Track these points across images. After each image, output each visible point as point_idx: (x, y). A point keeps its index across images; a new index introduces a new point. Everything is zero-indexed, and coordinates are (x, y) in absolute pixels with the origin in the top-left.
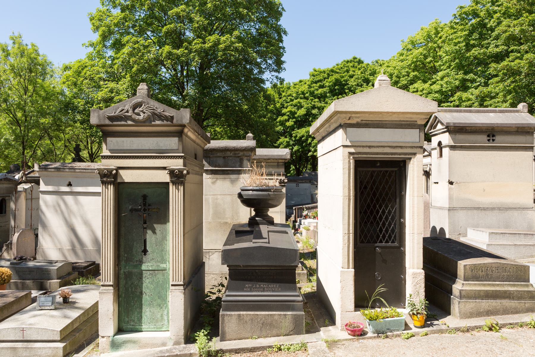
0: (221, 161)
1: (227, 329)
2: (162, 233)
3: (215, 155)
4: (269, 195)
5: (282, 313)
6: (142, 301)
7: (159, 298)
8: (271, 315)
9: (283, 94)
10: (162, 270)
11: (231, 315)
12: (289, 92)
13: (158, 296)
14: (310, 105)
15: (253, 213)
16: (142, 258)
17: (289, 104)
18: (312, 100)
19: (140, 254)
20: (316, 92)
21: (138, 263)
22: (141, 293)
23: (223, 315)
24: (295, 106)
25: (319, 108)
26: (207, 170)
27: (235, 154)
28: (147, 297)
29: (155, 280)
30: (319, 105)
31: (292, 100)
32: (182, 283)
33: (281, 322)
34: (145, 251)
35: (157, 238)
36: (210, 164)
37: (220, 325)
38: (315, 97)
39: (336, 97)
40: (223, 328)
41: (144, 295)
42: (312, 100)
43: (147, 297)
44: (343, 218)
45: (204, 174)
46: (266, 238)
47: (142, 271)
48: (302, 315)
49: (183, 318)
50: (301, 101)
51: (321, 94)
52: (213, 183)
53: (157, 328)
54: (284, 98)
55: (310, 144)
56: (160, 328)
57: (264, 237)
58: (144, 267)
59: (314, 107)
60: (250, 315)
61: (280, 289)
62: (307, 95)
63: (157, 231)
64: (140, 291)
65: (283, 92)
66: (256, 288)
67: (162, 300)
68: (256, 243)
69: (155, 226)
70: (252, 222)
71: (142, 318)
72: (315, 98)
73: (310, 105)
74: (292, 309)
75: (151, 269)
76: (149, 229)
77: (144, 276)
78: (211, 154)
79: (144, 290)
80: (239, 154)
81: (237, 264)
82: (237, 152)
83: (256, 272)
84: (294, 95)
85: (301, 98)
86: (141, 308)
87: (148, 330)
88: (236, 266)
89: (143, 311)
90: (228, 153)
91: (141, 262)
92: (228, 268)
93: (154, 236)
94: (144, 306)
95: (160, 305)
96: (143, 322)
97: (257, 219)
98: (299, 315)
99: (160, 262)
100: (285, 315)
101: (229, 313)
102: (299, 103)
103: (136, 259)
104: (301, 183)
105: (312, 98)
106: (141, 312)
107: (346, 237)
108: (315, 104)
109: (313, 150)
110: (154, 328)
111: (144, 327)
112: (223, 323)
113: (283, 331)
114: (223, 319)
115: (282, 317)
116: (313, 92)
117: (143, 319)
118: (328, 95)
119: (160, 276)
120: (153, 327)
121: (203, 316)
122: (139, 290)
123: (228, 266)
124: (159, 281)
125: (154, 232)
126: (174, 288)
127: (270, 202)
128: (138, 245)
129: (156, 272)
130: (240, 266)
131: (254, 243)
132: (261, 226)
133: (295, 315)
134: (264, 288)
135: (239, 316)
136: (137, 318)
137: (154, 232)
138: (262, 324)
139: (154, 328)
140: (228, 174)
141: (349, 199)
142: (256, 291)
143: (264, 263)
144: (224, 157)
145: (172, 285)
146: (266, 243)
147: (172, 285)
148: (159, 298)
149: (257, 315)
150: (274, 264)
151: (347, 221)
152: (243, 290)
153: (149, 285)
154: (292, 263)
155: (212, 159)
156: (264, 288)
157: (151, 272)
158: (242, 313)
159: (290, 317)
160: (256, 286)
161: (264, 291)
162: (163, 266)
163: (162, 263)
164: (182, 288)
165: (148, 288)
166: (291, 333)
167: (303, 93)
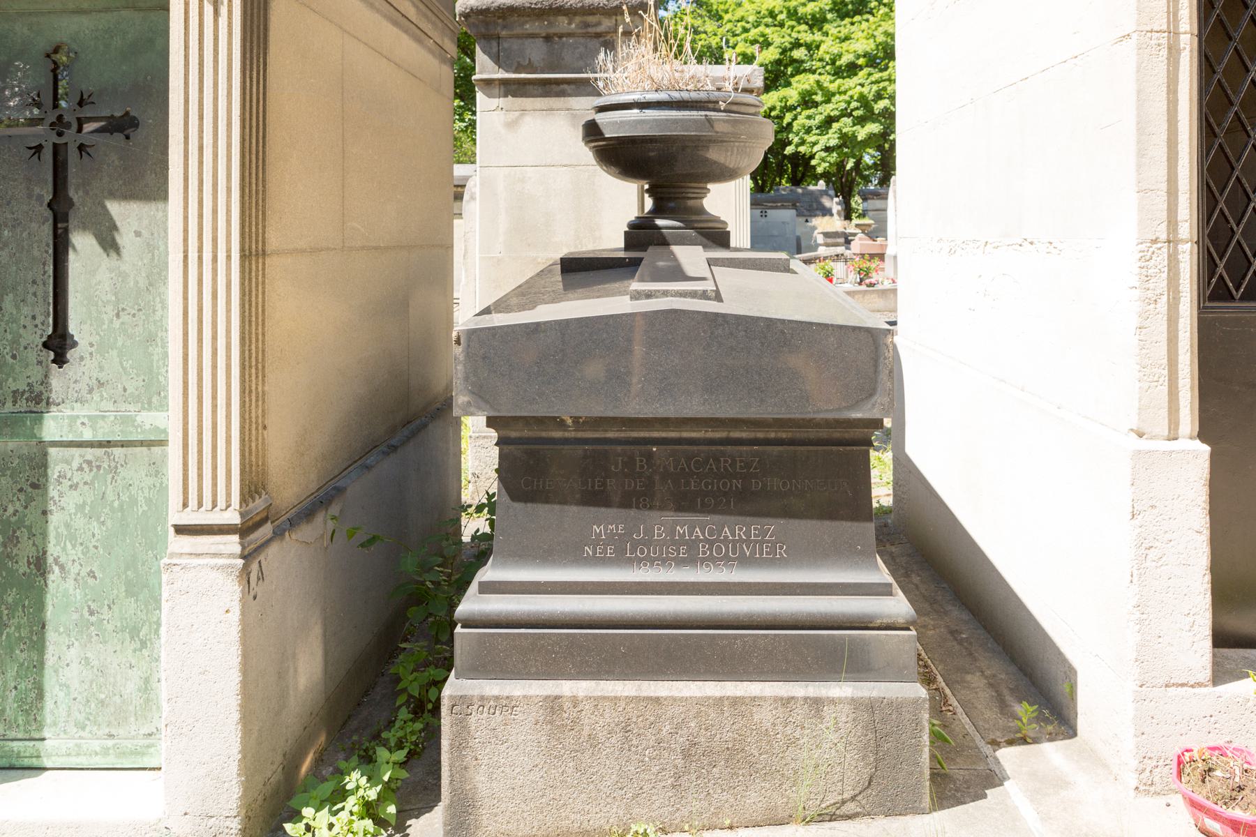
0: (536, 51)
1: (481, 781)
2: (151, 248)
3: (518, 31)
4: (709, 120)
5: (799, 690)
6: (40, 606)
7: (130, 593)
8: (735, 701)
9: (726, 17)
10: (149, 444)
11: (506, 704)
12: (740, 13)
13: (129, 584)
14: (787, 38)
15: (649, 203)
16: (45, 381)
17: (739, 38)
18: (793, 27)
19: (32, 356)
20: (801, 10)
21: (22, 405)
22: (40, 565)
23: (463, 701)
24: (754, 42)
25: (809, 47)
26: (488, 83)
27: (587, 25)
28: (70, 584)
29: (110, 496)
30: (807, 37)
31: (746, 30)
32: (232, 517)
33: (792, 742)
34: (59, 345)
35: (124, 276)
36: (497, 60)
37: (445, 757)
38: (800, 20)
39: (847, 20)
40: (462, 771)
41: (54, 577)
42: (793, 27)
43: (70, 584)
44: (1141, 154)
45: (479, 96)
46: (704, 279)
47: (43, 447)
48: (916, 702)
49: (236, 716)
50: (768, 31)
51: (813, 16)
52: (512, 125)
53: (122, 754)
54: (729, 26)
55: (790, 125)
56: (135, 753)
57: (690, 272)
58: (53, 427)
59: (797, 44)
60: (615, 700)
61: (781, 552)
62: (780, 17)
63: (125, 238)
64: (32, 552)
65: (726, 12)
66: (648, 543)
67: (135, 612)
68: (649, 295)
69: (115, 208)
70: (642, 235)
71: (40, 696)
72: (800, 24)
73: (787, 38)
74: (853, 664)
75: (88, 435)
76: (84, 227)
77: (54, 472)
78: (504, 27)
79: (53, 550)
80: (599, 24)
81: (541, 411)
82: (591, 19)
83: (650, 455)
84: (751, 19)
85: (767, 26)
86: (38, 644)
87: (73, 761)
88: (541, 421)
89: (50, 659)
90: (563, 24)
91: (38, 400)
92: (493, 434)
93: (105, 262)
94: (51, 636)
95: (134, 632)
96: (49, 719)
97: (659, 222)
98: (896, 706)
99: (137, 399)
100: (816, 704)
101: (492, 688)
102: (763, 35)
103: (12, 385)
104: (772, 208)
105: (794, 23)
106: (40, 665)
107: (1161, 259)
108: (800, 36)
109: (796, 140)
110: (106, 751)
111: (55, 745)
112: (460, 746)
113: (802, 795)
114: (462, 726)
115: (800, 713)
116: (796, 12)
117: (49, 703)
118: (829, 16)
119: (134, 468)
120: (96, 745)
121: (379, 671)
122: (26, 550)
123: (491, 422)
124: (134, 501)
125: (109, 243)
126: (187, 542)
127: (714, 154)
128: (26, 310)
129: (117, 451)
130: (561, 424)
131: (637, 296)
132: (676, 249)
133: (871, 706)
134: (692, 545)
135: (553, 704)
136: (21, 701)
137: (109, 243)
138: (686, 755)
139: (106, 751)
140: (562, 94)
141: (1173, 52)
142: (651, 561)
143: (695, 407)
144: (548, 38)
145: (181, 530)
146: (704, 295)
147: (181, 530)
148: (130, 593)
149: (657, 700)
150: (753, 413)
151: (1162, 172)
152: (576, 557)
153: (79, 522)
154: (855, 405)
155: (506, 45)
156: (692, 545)
157: (90, 453)
158: (567, 688)
159: (845, 714)
160: (649, 531)
161: (691, 560)
162: (149, 420)
163: (149, 406)
164: (232, 543)
165: (72, 538)
166: (851, 807)
167: (772, 14)
